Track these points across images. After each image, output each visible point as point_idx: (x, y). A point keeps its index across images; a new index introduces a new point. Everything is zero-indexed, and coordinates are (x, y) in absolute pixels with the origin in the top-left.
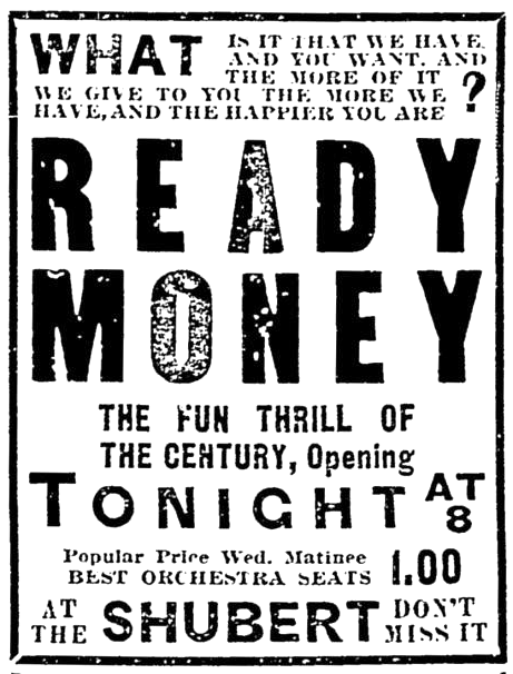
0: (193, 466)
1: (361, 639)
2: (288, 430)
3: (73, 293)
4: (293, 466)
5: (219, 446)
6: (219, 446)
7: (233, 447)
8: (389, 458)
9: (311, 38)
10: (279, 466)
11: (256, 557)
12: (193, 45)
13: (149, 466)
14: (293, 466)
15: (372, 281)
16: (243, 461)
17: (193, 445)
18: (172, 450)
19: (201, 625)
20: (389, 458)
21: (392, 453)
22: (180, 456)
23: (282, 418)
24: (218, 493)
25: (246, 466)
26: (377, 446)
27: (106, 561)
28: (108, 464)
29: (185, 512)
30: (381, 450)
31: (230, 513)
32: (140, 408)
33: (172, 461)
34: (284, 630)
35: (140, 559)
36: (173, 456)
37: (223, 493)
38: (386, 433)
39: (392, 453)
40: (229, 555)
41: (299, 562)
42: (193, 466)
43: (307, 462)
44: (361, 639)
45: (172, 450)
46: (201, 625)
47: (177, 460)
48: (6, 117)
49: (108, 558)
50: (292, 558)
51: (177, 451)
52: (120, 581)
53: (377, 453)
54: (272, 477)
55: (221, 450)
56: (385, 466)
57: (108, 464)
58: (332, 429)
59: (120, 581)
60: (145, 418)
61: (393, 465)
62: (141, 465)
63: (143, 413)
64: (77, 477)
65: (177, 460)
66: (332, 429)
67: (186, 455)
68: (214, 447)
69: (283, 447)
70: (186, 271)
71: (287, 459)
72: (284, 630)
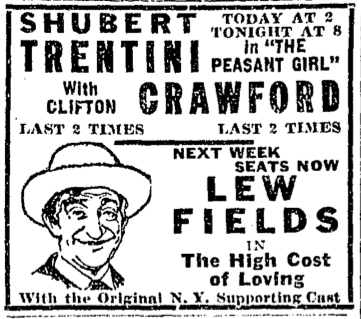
0: (230, 70)
2: (79, 83)
12: (191, 19)
15: (85, 44)
17: (230, 60)
24: (200, 68)
25: (101, 112)
27: (289, 296)
29: (287, 185)
30: (282, 295)
31: (283, 223)
40: (25, 296)
42: (230, 70)
48: (11, 225)
49: (287, 280)
52: (59, 133)
58: (65, 112)
59: (59, 133)
60: (302, 45)
66: (65, 112)
70: (72, 189)
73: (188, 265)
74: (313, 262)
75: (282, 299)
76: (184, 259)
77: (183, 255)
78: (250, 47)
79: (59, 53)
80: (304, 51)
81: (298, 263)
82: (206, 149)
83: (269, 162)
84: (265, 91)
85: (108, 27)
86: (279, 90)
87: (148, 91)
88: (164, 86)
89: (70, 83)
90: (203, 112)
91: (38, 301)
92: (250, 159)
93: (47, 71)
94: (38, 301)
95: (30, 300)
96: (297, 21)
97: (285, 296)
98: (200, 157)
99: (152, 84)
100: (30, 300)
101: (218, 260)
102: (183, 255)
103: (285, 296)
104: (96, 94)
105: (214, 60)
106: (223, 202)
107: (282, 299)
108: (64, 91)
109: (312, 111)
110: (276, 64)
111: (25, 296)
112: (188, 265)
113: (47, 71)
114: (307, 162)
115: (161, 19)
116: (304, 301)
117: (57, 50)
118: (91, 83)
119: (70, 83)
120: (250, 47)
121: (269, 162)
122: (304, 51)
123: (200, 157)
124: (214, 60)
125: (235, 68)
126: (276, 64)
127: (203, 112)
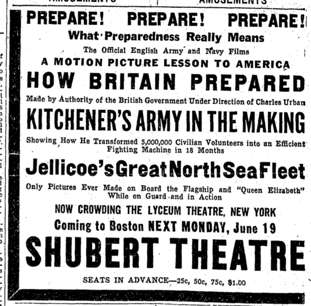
4: (228, 232)
5: (74, 59)
7: (217, 113)
10: (223, 231)
13: (141, 213)
14: (228, 232)
16: (262, 214)
18: (71, 168)
21: (83, 224)
22: (163, 210)
23: (199, 254)
26: (77, 221)
28: (129, 213)
32: (139, 207)
33: (71, 171)
35: (97, 188)
38: (229, 67)
39: (83, 224)
43: (78, 211)
45: (71, 168)
47: (59, 226)
51: (62, 115)
53: (77, 224)
54: (219, 236)
55: (130, 78)
57: (189, 214)
60: (140, 210)
62: (138, 213)
63: (140, 208)
64: (101, 159)
65: (82, 211)
66: (104, 129)
67: (165, 210)
71: (226, 229)
73: (218, 66)
74: (235, 169)
76: (174, 246)
77: (215, 61)
79: (98, 248)
81: (281, 66)
84: (119, 247)
85: (95, 84)
86: (194, 225)
87: (58, 222)
88: (45, 239)
89: (69, 205)
90: (242, 269)
93: (171, 239)
96: (201, 199)
99: (32, 237)
101: (177, 189)
102: (215, 61)
106: (182, 113)
110: (143, 249)
112: (218, 66)
113: (171, 239)
114: (96, 65)
115: (266, 63)
116: (196, 148)
117: (97, 246)
118: (213, 163)
119: (69, 205)
124: (109, 60)
125: (204, 213)
126: (143, 249)
127: (242, 269)
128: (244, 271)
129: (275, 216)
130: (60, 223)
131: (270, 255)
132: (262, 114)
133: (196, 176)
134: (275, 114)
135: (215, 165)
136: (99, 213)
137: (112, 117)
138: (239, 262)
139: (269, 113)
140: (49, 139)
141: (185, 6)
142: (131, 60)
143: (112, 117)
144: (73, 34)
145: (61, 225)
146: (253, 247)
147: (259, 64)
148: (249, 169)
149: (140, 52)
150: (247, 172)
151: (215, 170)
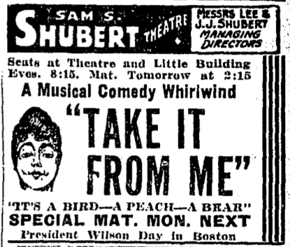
1: (191, 194)
3: (199, 162)
6: (190, 111)
8: (222, 92)
9: (89, 96)
11: (140, 64)
18: (103, 88)
19: (236, 25)
20: (222, 92)
33: (103, 93)
34: (38, 222)
36: (103, 91)
37: (10, 242)
40: (92, 233)
41: (98, 77)
44: (191, 194)
45: (103, 88)
46: (236, 25)
50: (94, 75)
53: (186, 90)
56: (220, 96)
61: (53, 88)
68: (186, 112)
69: (154, 90)
72: (38, 222)
75: (175, 237)
78: (218, 91)
80: (229, 193)
82: (234, 217)
83: (123, 216)
91: (103, 238)
92: (218, 213)
94: (103, 238)
95: (96, 237)
97: (177, 236)
98: (228, 225)
100: (96, 237)
103: (177, 236)
104: (166, 193)
105: (234, 96)
107: (175, 237)
108: (163, 93)
109: (167, 194)
111: (92, 233)
118: (178, 86)
120: (218, 91)
121: (123, 216)
122: (229, 193)
123: (228, 225)
124: (234, 96)
128: (128, 149)
129: (52, 191)
130: (106, 88)
131: (120, 4)
132: (112, 114)
133: (191, 97)
134: (138, 112)
135: (180, 88)
136: (171, 96)
137: (113, 170)
138: (67, 223)
139: (127, 111)
140: (220, 89)
141: (4, 116)
142: (170, 74)
143: (113, 170)
144: (46, 88)
145: (108, 91)
146: (124, 219)
147: (221, 221)
148: (81, 89)
149: (207, 63)
150: (79, 92)
151: (180, 92)
